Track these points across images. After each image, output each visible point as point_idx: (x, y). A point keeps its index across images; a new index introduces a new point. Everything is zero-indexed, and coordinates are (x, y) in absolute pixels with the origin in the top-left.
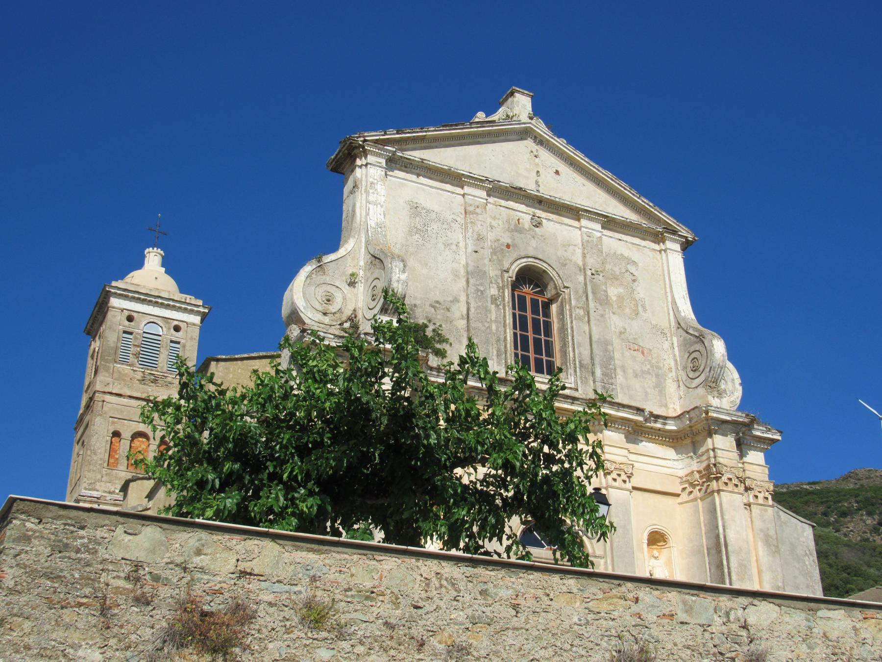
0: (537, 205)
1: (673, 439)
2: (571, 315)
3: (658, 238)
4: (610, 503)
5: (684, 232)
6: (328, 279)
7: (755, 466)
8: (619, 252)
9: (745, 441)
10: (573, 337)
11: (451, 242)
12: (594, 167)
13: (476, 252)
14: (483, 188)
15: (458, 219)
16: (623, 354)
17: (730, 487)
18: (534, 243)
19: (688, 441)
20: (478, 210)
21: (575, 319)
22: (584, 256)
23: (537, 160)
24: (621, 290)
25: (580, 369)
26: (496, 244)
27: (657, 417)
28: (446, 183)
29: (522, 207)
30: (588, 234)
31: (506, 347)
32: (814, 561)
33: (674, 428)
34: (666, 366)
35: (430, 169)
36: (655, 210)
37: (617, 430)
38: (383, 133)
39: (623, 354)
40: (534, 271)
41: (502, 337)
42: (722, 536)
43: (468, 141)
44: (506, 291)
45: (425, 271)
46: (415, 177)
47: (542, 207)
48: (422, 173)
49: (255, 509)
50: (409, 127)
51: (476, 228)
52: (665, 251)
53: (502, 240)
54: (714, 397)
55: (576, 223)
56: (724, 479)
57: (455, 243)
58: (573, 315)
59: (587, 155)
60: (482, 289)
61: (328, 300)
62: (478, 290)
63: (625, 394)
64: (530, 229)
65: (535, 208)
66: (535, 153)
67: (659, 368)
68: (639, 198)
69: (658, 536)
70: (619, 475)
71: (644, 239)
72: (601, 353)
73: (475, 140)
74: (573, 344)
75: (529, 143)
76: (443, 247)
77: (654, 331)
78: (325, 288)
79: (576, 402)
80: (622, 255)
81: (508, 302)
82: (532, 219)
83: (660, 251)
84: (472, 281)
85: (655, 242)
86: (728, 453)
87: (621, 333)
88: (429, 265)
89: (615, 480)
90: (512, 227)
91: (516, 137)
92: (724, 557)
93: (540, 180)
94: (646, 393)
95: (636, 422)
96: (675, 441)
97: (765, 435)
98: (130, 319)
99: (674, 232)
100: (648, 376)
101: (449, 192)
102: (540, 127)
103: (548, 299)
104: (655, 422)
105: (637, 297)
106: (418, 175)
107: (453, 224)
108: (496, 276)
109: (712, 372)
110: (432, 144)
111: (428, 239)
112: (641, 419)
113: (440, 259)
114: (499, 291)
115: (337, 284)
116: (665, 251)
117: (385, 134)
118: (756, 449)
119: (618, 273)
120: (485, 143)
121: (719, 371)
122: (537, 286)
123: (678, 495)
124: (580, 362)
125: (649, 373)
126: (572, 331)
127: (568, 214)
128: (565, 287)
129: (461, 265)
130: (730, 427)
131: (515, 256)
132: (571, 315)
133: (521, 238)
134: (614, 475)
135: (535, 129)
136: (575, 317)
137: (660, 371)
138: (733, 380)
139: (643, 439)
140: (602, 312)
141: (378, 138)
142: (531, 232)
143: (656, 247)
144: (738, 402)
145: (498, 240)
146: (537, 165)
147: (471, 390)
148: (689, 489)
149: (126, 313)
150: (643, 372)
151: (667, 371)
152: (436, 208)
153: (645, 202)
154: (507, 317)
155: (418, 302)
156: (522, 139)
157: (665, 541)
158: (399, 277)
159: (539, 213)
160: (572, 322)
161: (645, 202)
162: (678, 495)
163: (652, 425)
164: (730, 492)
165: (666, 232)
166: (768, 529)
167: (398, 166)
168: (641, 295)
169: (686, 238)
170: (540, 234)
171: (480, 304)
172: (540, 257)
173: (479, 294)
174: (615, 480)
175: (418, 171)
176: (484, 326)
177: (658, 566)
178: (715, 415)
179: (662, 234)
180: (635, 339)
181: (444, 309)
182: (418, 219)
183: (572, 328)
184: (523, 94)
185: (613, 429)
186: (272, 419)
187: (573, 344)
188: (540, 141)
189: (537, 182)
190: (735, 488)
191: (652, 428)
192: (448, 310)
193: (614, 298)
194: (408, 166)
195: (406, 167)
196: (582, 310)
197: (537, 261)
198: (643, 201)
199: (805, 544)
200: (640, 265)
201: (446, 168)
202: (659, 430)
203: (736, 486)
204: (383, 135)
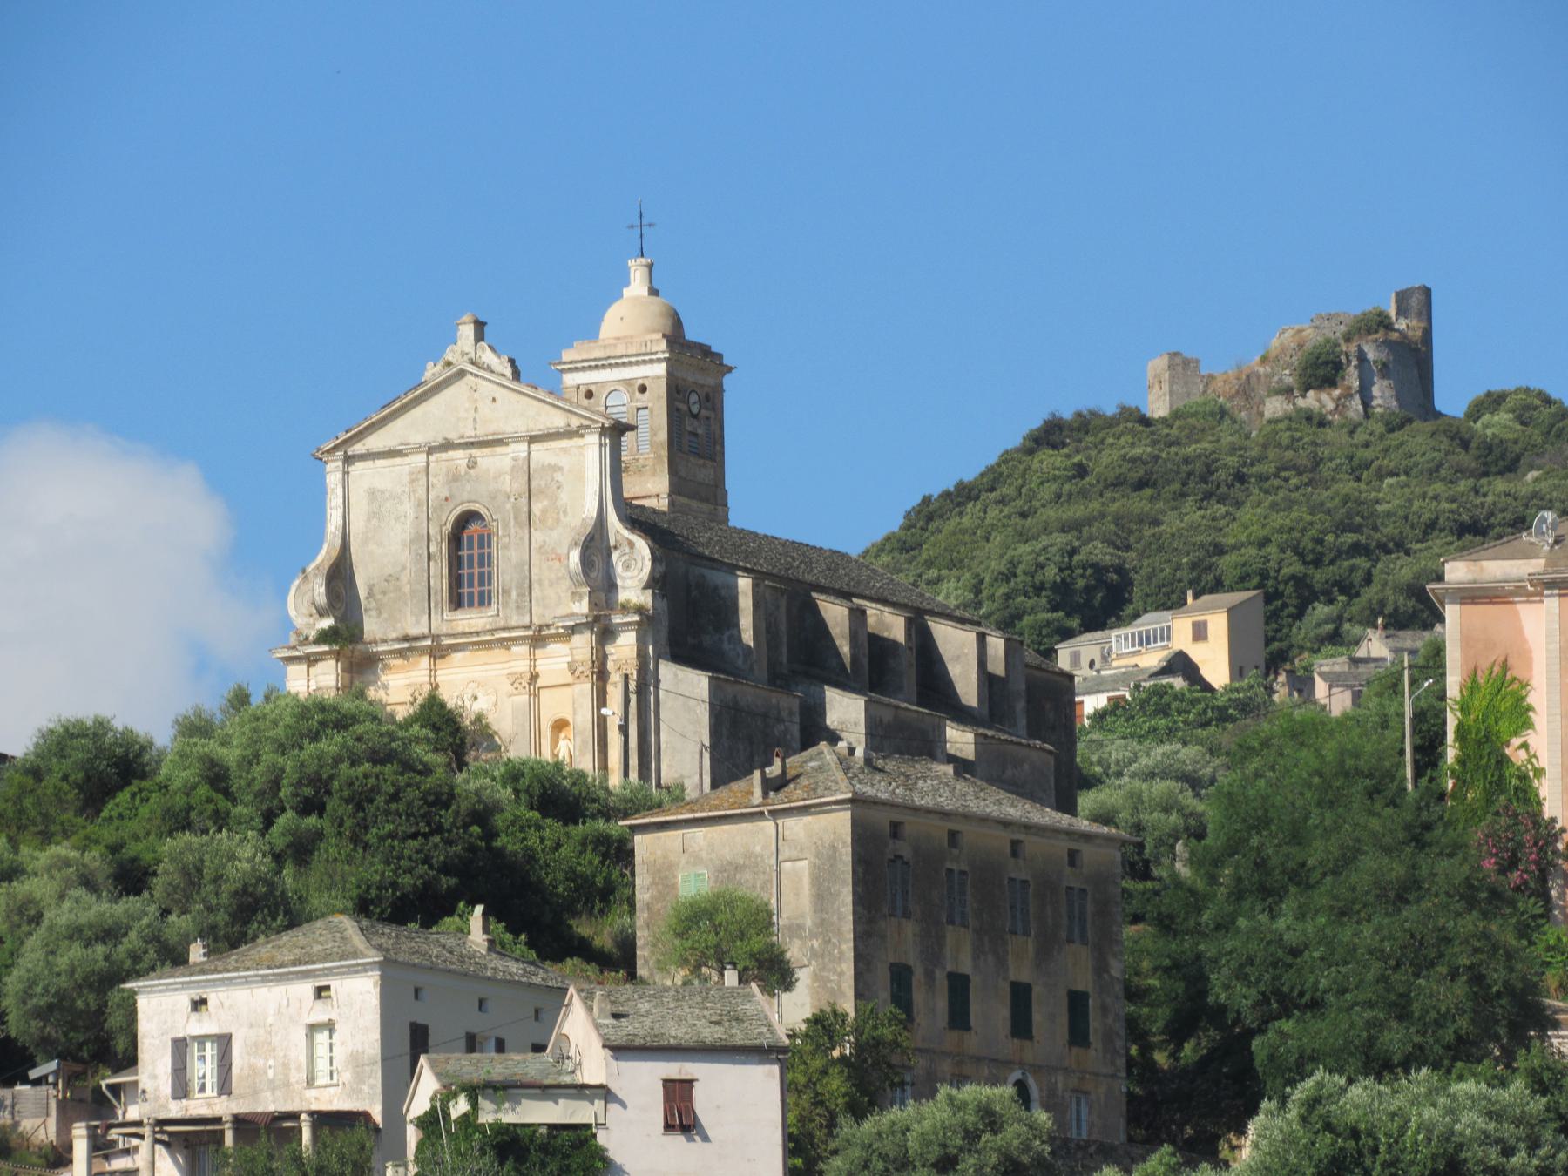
23: (476, 395)
49: (386, 740)
94: (559, 597)
98: (589, 395)
131: (452, 506)
138: (643, 558)
146: (476, 400)
149: (583, 390)
150: (558, 579)
186: (297, 722)
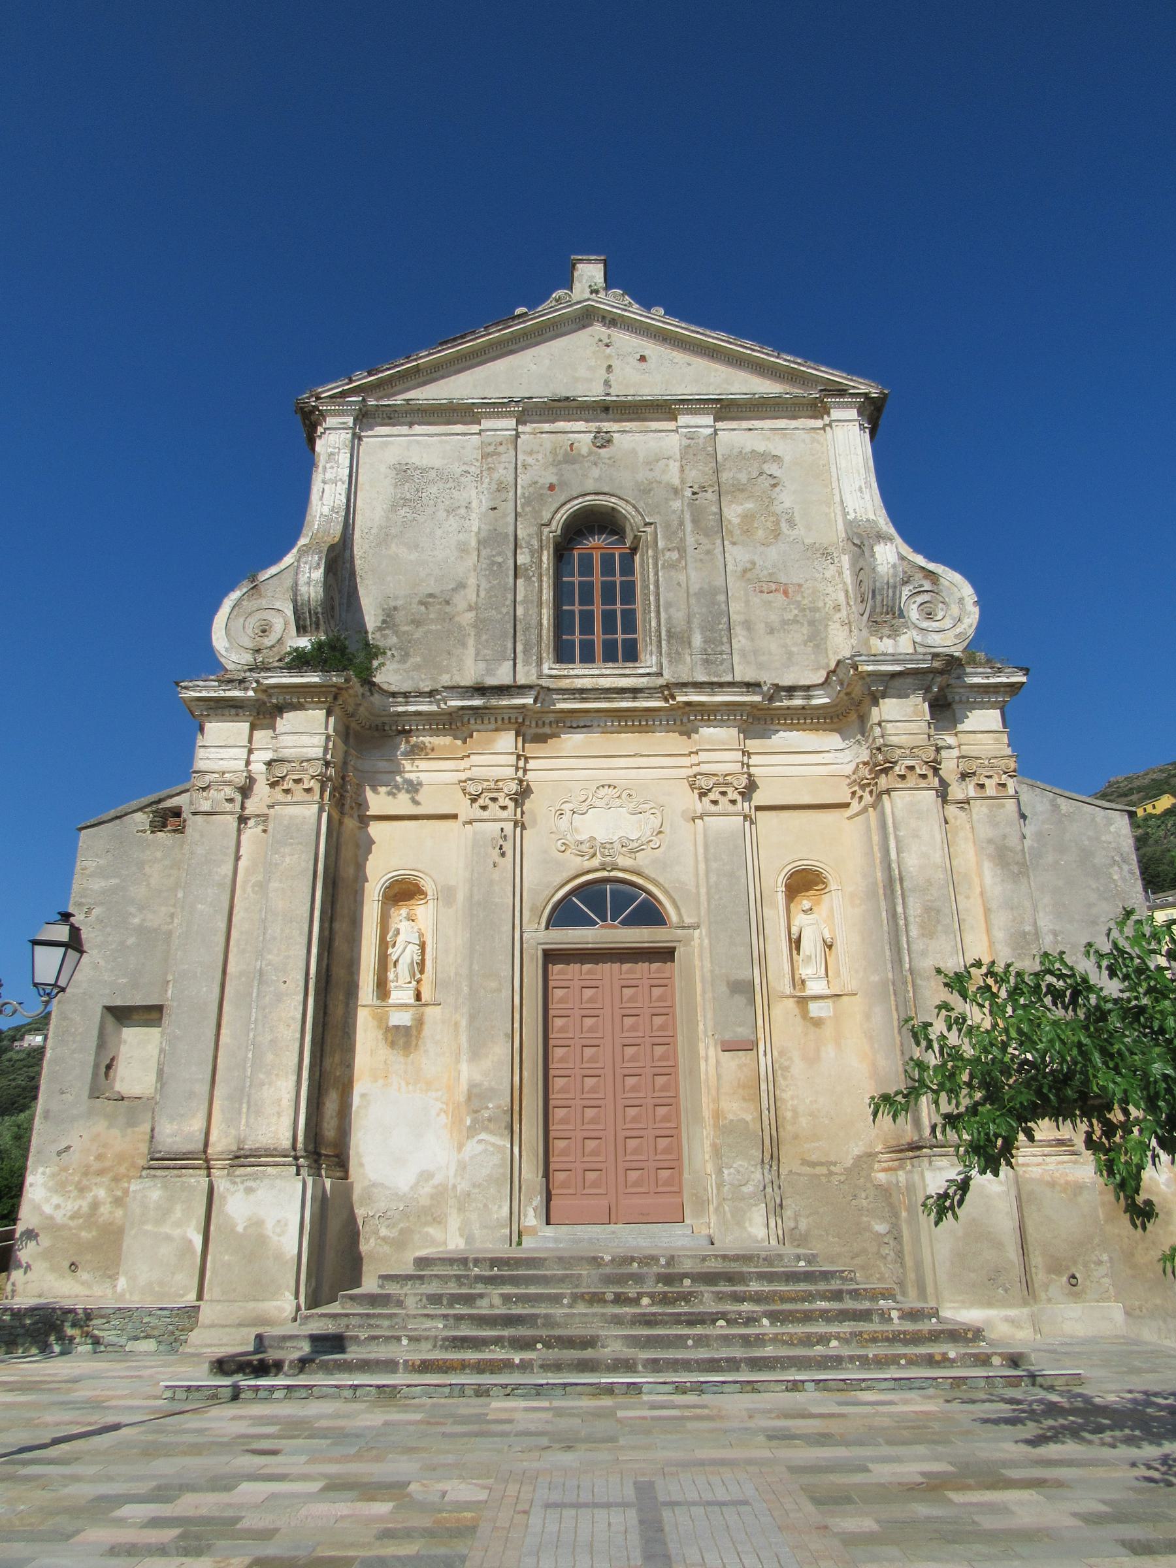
0: (603, 415)
1: (832, 718)
2: (656, 564)
3: (817, 409)
4: (85, 948)
5: (863, 386)
6: (264, 603)
7: (979, 735)
8: (748, 449)
9: (957, 698)
10: (657, 595)
11: (457, 505)
12: (698, 333)
13: (495, 508)
14: (508, 414)
15: (472, 469)
16: (747, 602)
17: (912, 781)
18: (595, 472)
19: (853, 716)
20: (501, 449)
21: (663, 567)
22: (682, 470)
23: (608, 350)
24: (749, 505)
25: (669, 642)
26: (531, 489)
27: (791, 690)
28: (455, 424)
29: (580, 425)
30: (688, 435)
31: (540, 636)
32: (1131, 872)
33: (827, 700)
34: (830, 604)
35: (425, 411)
36: (809, 367)
37: (722, 723)
38: (347, 381)
39: (747, 602)
40: (602, 513)
41: (534, 622)
42: (894, 866)
43: (492, 354)
44: (545, 553)
45: (413, 556)
46: (407, 427)
47: (611, 416)
48: (416, 419)
50: (386, 361)
51: (496, 476)
52: (830, 425)
53: (541, 481)
54: (881, 638)
55: (671, 425)
56: (899, 769)
57: (464, 504)
58: (660, 563)
59: (682, 319)
60: (500, 559)
61: (264, 631)
62: (493, 563)
63: (748, 663)
64: (590, 453)
65: (601, 421)
66: (606, 341)
67: (815, 610)
68: (777, 358)
69: (811, 877)
70: (724, 794)
71: (795, 418)
72: (704, 610)
73: (505, 350)
74: (658, 607)
75: (598, 329)
76: (445, 514)
77: (809, 553)
78: (259, 615)
79: (639, 695)
80: (753, 451)
81: (548, 569)
82: (595, 437)
83: (823, 429)
84: (484, 553)
85: (815, 418)
86: (907, 724)
87: (745, 571)
88: (421, 545)
89: (715, 802)
90: (560, 457)
91: (574, 326)
92: (900, 901)
93: (612, 377)
94: (790, 655)
95: (753, 705)
96: (835, 720)
97: (992, 680)
99: (842, 392)
100: (796, 627)
101: (458, 434)
102: (615, 302)
103: (630, 548)
104: (791, 697)
105: (778, 509)
106: (411, 425)
107: (463, 479)
108: (529, 535)
109: (878, 598)
110: (434, 375)
111: (422, 509)
112: (757, 698)
113: (439, 532)
114: (532, 557)
115: (277, 605)
116: (830, 425)
117: (351, 381)
118: (982, 706)
119: (744, 481)
120: (523, 349)
121: (891, 594)
122: (615, 533)
123: (847, 805)
124: (668, 631)
125: (795, 621)
126: (657, 586)
127: (656, 415)
128: (647, 524)
129: (473, 534)
130: (909, 680)
132: (656, 564)
133: (574, 470)
134: (713, 796)
135: (598, 305)
136: (664, 564)
137: (817, 615)
139: (778, 727)
140: (709, 547)
141: (340, 389)
142: (592, 458)
143: (819, 423)
144: (971, 632)
145: (536, 483)
146: (609, 357)
147: (461, 713)
148: (860, 793)
150: (785, 622)
151: (832, 612)
152: (438, 463)
153: (788, 361)
154: (545, 591)
155: (399, 603)
156: (584, 327)
157: (824, 883)
158: (309, 578)
159: (606, 426)
160: (656, 574)
161: (788, 361)
162: (847, 805)
163: (786, 703)
164: (910, 789)
165: (826, 396)
166: (1005, 837)
167: (379, 420)
168: (787, 504)
169: (866, 395)
170: (607, 456)
171: (495, 582)
172: (606, 490)
173: (495, 568)
174: (715, 802)
175: (409, 419)
176: (500, 613)
177: (808, 925)
178: (870, 668)
179: (822, 401)
180: (771, 575)
181: (440, 603)
182: (407, 485)
183: (657, 582)
184: (589, 261)
185: (715, 723)
187: (658, 607)
188: (612, 321)
189: (607, 383)
190: (921, 780)
191: (788, 708)
192: (448, 603)
193: (736, 521)
194: (392, 417)
195: (390, 418)
196: (676, 552)
197: (600, 497)
198: (786, 360)
199: (1113, 845)
200: (787, 459)
201: (445, 401)
202: (803, 708)
203: (733, 802)
204: (348, 384)
